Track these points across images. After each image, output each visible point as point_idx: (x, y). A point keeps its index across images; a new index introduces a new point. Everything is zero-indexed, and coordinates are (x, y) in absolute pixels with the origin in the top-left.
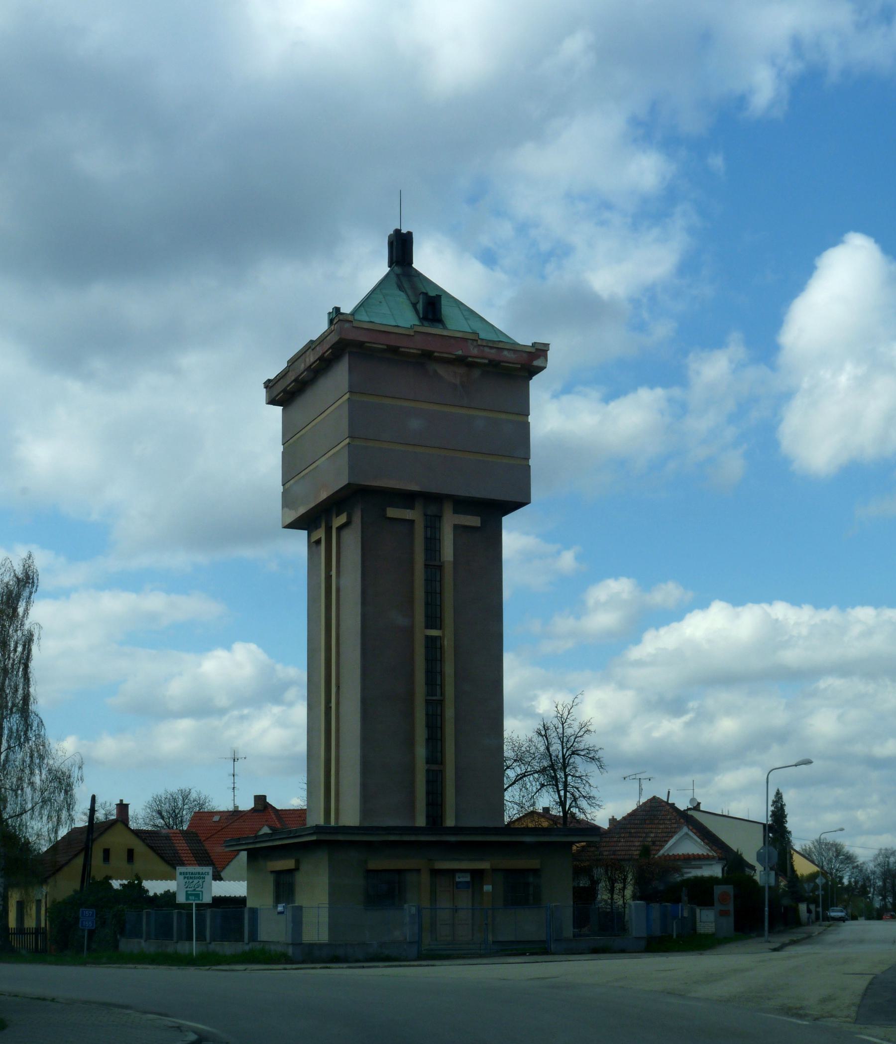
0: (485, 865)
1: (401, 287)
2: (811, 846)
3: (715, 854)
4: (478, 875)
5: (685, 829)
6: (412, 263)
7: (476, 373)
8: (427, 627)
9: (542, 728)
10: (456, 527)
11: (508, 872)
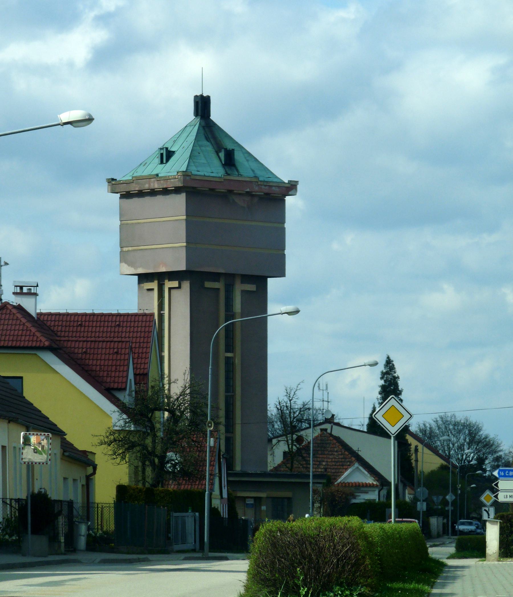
0: (263, 495)
1: (207, 139)
2: (434, 425)
3: (378, 484)
4: (258, 500)
5: (357, 465)
6: (210, 116)
7: (256, 200)
8: (233, 358)
9: (278, 404)
10: (243, 292)
11: (273, 498)
